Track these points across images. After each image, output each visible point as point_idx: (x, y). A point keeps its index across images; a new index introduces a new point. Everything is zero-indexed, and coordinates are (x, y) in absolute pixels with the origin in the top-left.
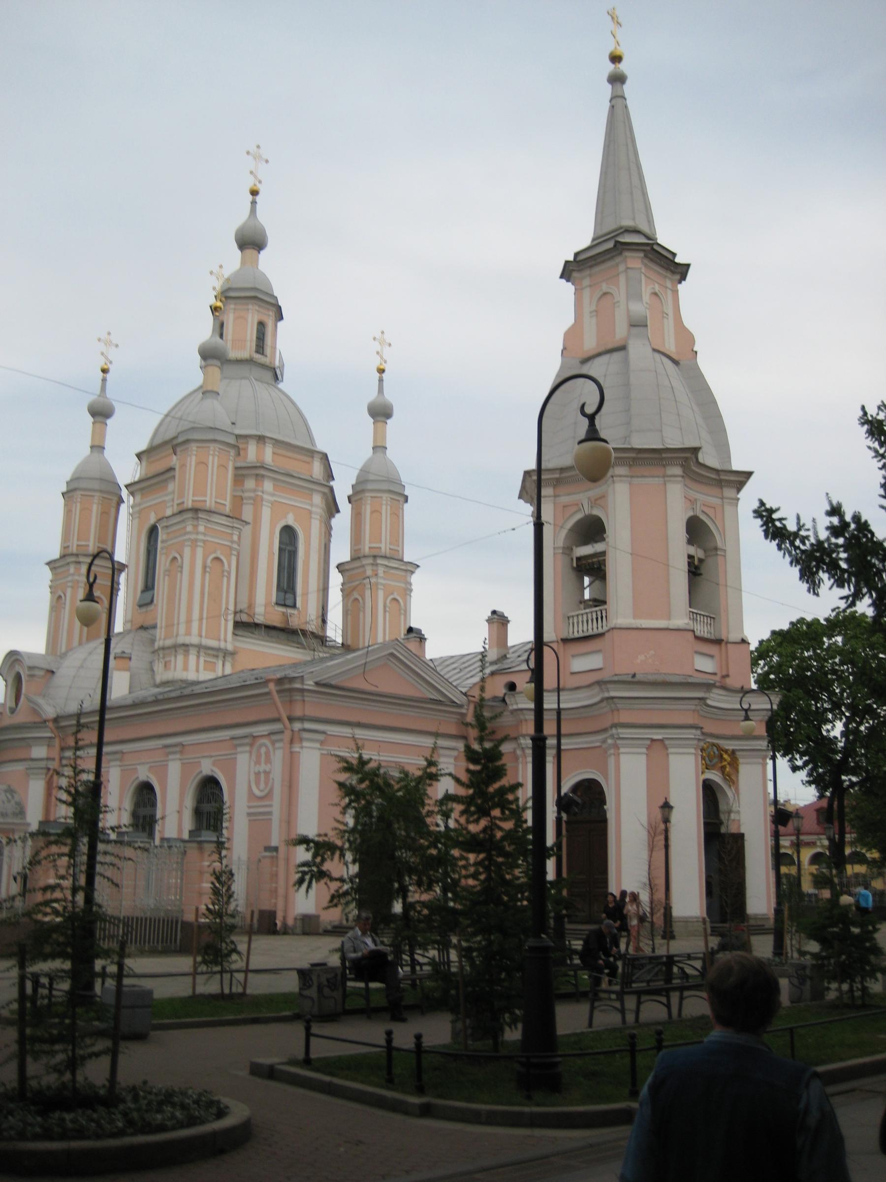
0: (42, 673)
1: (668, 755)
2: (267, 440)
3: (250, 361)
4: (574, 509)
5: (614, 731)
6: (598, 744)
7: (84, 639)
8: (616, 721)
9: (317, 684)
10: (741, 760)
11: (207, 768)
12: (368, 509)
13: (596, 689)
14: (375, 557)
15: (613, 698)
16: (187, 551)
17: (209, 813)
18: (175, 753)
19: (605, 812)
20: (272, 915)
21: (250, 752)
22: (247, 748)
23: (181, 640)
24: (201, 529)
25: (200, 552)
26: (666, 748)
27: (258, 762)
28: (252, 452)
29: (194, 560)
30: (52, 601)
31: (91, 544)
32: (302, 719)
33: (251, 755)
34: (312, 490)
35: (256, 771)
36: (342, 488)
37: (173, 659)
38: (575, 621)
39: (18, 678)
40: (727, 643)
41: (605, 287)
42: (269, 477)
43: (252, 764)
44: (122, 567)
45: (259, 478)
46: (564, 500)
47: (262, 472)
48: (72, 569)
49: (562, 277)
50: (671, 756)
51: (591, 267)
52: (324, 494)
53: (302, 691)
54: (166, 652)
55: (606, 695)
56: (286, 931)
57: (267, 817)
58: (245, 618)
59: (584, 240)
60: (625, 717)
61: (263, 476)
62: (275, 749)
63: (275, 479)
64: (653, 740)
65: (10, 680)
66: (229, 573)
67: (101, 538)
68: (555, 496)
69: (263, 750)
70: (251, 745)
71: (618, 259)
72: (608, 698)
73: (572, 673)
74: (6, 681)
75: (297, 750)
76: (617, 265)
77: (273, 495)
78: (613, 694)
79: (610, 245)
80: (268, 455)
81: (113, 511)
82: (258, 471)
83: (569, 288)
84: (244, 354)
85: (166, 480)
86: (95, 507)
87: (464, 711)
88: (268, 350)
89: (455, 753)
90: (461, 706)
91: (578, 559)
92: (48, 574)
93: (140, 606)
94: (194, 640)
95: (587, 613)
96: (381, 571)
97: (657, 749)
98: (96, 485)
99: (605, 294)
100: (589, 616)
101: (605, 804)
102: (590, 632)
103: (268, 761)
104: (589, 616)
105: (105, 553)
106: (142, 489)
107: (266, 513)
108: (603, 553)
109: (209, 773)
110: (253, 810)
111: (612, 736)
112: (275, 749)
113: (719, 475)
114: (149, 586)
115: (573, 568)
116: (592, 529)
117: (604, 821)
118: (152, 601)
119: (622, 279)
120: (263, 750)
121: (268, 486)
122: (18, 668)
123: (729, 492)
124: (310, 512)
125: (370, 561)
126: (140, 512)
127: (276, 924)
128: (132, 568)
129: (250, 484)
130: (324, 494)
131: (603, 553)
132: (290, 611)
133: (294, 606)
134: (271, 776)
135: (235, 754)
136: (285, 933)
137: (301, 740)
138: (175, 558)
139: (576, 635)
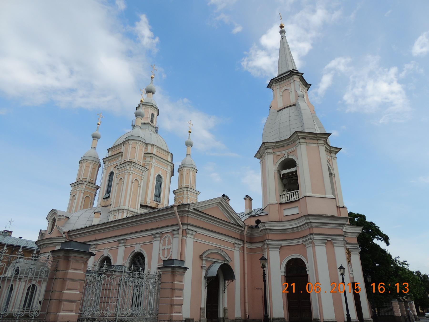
0: (64, 218)
1: (334, 247)
3: (149, 124)
4: (281, 156)
5: (311, 236)
8: (312, 232)
9: (194, 209)
10: (351, 253)
11: (137, 249)
12: (185, 173)
13: (304, 218)
14: (187, 188)
15: (311, 222)
16: (126, 176)
18: (122, 243)
19: (306, 272)
22: (159, 239)
23: (122, 207)
24: (132, 169)
25: (131, 176)
27: (164, 245)
28: (149, 150)
29: (129, 179)
30: (71, 198)
31: (88, 178)
32: (187, 224)
33: (160, 242)
35: (163, 249)
36: (177, 165)
37: (117, 214)
38: (288, 196)
39: (54, 220)
40: (339, 207)
41: (285, 88)
43: (161, 245)
44: (98, 188)
46: (277, 153)
47: (153, 155)
48: (80, 186)
50: (335, 247)
51: (280, 82)
52: (171, 166)
53: (188, 211)
54: (115, 212)
55: (308, 221)
58: (143, 204)
60: (315, 231)
62: (173, 238)
64: (328, 241)
65: (51, 221)
66: (140, 185)
67: (92, 176)
69: (167, 239)
70: (161, 237)
71: (290, 79)
72: (308, 223)
74: (48, 221)
76: (290, 80)
77: (155, 164)
78: (311, 221)
79: (289, 73)
80: (155, 151)
81: (97, 168)
84: (147, 122)
85: (118, 157)
86: (91, 166)
87: (243, 229)
88: (154, 122)
89: (240, 246)
90: (242, 227)
91: (282, 175)
92: (70, 188)
94: (126, 208)
96: (189, 193)
97: (330, 244)
98: (92, 159)
100: (288, 195)
103: (169, 243)
104: (288, 195)
105: (92, 183)
106: (109, 160)
107: (153, 170)
108: (296, 172)
109: (139, 251)
111: (311, 239)
112: (173, 238)
114: (108, 191)
115: (281, 178)
116: (290, 163)
117: (307, 276)
119: (292, 85)
121: (154, 160)
122: (54, 216)
123: (333, 155)
124: (167, 172)
125: (186, 189)
126: (107, 168)
128: (102, 189)
129: (148, 159)
130: (171, 166)
131: (296, 172)
132: (158, 203)
133: (160, 202)
134: (171, 251)
135: (153, 242)
137: (186, 234)
139: (285, 202)
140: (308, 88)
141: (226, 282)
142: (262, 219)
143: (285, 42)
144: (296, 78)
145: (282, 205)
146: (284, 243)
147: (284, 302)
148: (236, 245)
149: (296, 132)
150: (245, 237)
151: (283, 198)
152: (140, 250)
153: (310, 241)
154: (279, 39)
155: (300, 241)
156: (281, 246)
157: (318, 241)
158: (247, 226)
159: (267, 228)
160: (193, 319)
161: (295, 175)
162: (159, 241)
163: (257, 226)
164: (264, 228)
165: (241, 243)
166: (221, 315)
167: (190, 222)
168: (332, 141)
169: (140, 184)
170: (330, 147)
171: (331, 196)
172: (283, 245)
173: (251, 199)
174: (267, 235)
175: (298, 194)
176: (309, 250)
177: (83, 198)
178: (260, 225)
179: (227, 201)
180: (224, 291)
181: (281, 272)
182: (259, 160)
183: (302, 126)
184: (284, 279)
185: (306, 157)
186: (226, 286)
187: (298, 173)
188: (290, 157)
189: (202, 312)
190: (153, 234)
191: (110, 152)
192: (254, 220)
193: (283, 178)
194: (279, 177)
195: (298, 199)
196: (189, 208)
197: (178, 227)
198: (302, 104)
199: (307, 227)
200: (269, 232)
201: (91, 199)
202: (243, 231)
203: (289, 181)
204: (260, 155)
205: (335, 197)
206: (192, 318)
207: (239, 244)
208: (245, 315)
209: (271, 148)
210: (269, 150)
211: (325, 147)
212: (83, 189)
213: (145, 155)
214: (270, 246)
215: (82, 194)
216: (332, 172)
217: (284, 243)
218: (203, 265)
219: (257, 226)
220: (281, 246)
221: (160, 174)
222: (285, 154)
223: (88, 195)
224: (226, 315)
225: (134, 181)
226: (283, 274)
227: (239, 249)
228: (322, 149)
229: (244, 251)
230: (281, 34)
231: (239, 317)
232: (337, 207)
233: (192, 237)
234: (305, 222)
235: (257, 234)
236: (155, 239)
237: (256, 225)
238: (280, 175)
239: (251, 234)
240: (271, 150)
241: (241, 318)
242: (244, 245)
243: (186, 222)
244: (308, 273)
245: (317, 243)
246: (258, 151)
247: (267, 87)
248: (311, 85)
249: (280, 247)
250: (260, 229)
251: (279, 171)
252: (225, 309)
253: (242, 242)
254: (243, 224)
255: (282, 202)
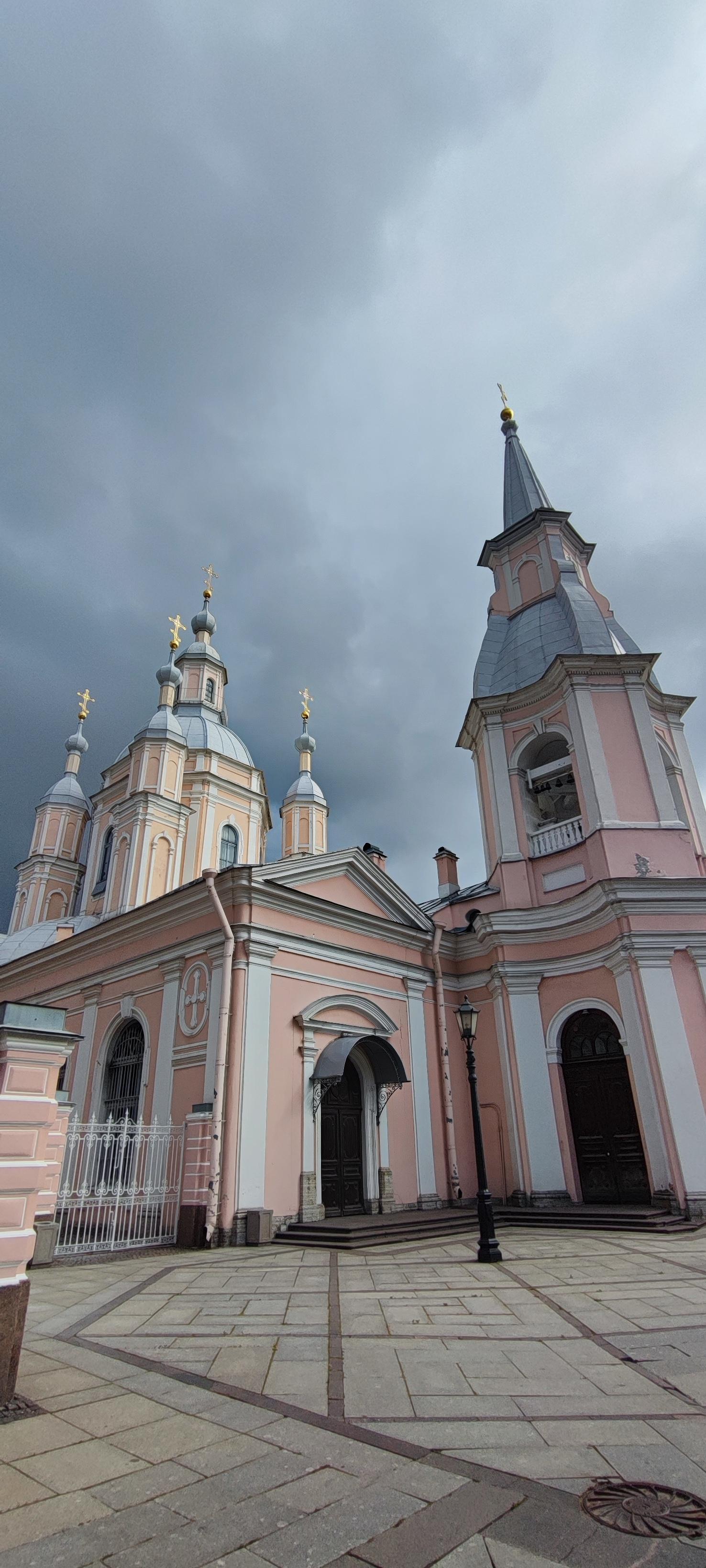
1: (695, 969)
2: (213, 755)
4: (525, 732)
6: (601, 964)
7: (36, 919)
9: (268, 882)
15: (620, 901)
17: (126, 1068)
19: (620, 1048)
20: (200, 1212)
21: (180, 979)
22: (177, 975)
26: (692, 960)
27: (190, 992)
34: (250, 799)
35: (187, 1003)
38: (541, 839)
41: (525, 558)
42: (213, 783)
43: (183, 993)
45: (205, 782)
46: (514, 725)
47: (209, 778)
48: (37, 869)
49: (480, 564)
55: (612, 897)
56: (222, 1239)
57: (201, 1053)
59: (498, 529)
61: (209, 782)
63: (218, 785)
68: (504, 723)
69: (197, 974)
70: (182, 970)
71: (536, 532)
73: (545, 893)
75: (243, 966)
78: (621, 895)
79: (531, 518)
82: (205, 778)
83: (487, 573)
87: (429, 938)
89: (423, 987)
90: (426, 932)
91: (534, 781)
93: (94, 895)
95: (572, 823)
99: (526, 562)
101: (619, 1037)
102: (561, 847)
106: (103, 799)
107: (211, 811)
108: (570, 767)
110: (179, 1057)
111: (624, 948)
113: (662, 701)
115: (528, 790)
116: (553, 747)
118: (104, 891)
119: (542, 547)
120: (197, 974)
123: (671, 718)
127: (205, 1230)
129: (197, 787)
130: (260, 803)
131: (570, 767)
135: (83, 1008)
136: (220, 1244)
137: (247, 954)
138: (125, 839)
140: (589, 555)
141: (384, 1091)
142: (482, 906)
143: (517, 448)
144: (553, 531)
145: (544, 866)
146: (551, 970)
147: (561, 1142)
148: (410, 984)
149: (558, 655)
150: (438, 961)
151: (539, 843)
152: (133, 1011)
153: (623, 954)
154: (503, 446)
155: (594, 960)
156: (543, 979)
157: (646, 953)
158: (442, 927)
159: (496, 928)
160: (270, 1213)
161: (567, 779)
162: (177, 983)
163: (470, 929)
164: (489, 929)
165: (426, 978)
166: (372, 1191)
167: (257, 922)
168: (668, 678)
169: (173, 847)
170: (661, 694)
171: (676, 823)
172: (546, 975)
173: (453, 858)
174: (500, 950)
175: (580, 828)
176: (623, 983)
177: (45, 899)
178: (477, 924)
179: (376, 861)
180: (378, 1117)
181: (547, 1053)
182: (470, 753)
183: (578, 643)
184: (556, 1073)
185: (592, 724)
186: (383, 1101)
187: (574, 771)
188: (550, 730)
189: (305, 1186)
190: (161, 964)
191: (108, 780)
192: (461, 911)
193: (536, 790)
194: (524, 788)
195: (580, 840)
196: (250, 880)
197: (222, 938)
198: (571, 590)
199: (611, 914)
200: (505, 940)
201: (66, 900)
202: (430, 943)
203: (553, 793)
204: (468, 738)
205: (686, 822)
206: (266, 1208)
207: (425, 982)
208: (450, 1185)
209: (495, 713)
210: (490, 720)
211: (648, 698)
212: (45, 876)
213: (188, 778)
214: (509, 981)
215: (43, 888)
216: (674, 764)
217: (551, 970)
218: (306, 1045)
219: (470, 929)
220: (543, 979)
221: (232, 823)
222: (534, 725)
223: (59, 890)
224: (387, 1189)
225: (156, 841)
226: (554, 1059)
227: (420, 995)
228: (639, 699)
229: (435, 998)
230: (505, 434)
231: (431, 1196)
232: (698, 857)
233: (267, 962)
234: (604, 900)
235: (472, 948)
236: (167, 978)
237: (466, 924)
238: (527, 782)
239: (456, 950)
240: (497, 718)
241: (436, 1195)
242: (435, 982)
243: (245, 921)
244: (626, 1052)
245: (643, 958)
246: (464, 727)
247: (479, 564)
248: (593, 546)
249: (538, 980)
250: (480, 935)
251: (522, 772)
252: (381, 1173)
253: (427, 974)
254: (429, 924)
255: (537, 855)
